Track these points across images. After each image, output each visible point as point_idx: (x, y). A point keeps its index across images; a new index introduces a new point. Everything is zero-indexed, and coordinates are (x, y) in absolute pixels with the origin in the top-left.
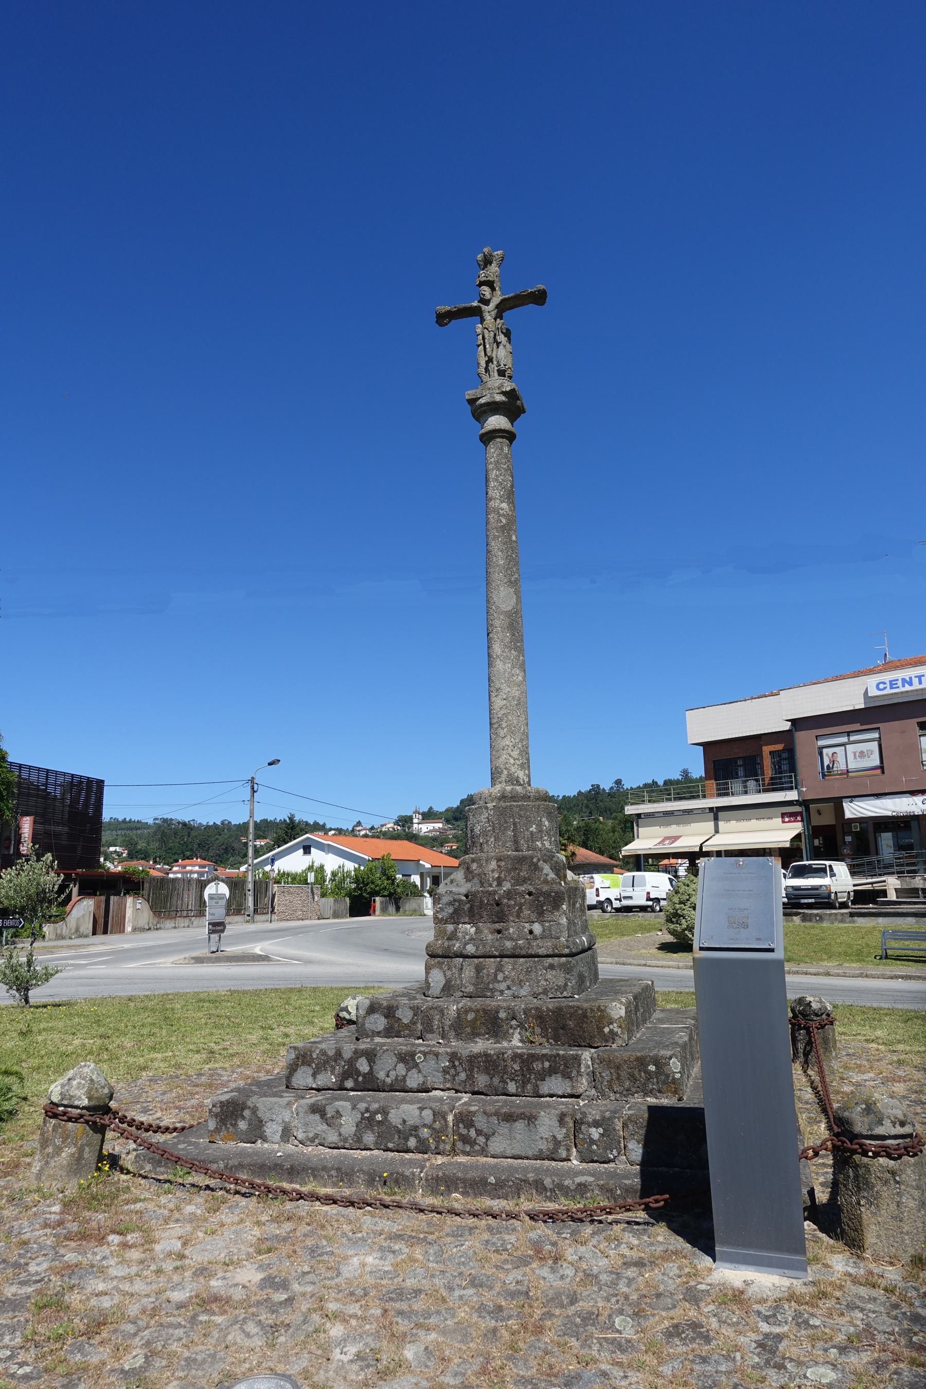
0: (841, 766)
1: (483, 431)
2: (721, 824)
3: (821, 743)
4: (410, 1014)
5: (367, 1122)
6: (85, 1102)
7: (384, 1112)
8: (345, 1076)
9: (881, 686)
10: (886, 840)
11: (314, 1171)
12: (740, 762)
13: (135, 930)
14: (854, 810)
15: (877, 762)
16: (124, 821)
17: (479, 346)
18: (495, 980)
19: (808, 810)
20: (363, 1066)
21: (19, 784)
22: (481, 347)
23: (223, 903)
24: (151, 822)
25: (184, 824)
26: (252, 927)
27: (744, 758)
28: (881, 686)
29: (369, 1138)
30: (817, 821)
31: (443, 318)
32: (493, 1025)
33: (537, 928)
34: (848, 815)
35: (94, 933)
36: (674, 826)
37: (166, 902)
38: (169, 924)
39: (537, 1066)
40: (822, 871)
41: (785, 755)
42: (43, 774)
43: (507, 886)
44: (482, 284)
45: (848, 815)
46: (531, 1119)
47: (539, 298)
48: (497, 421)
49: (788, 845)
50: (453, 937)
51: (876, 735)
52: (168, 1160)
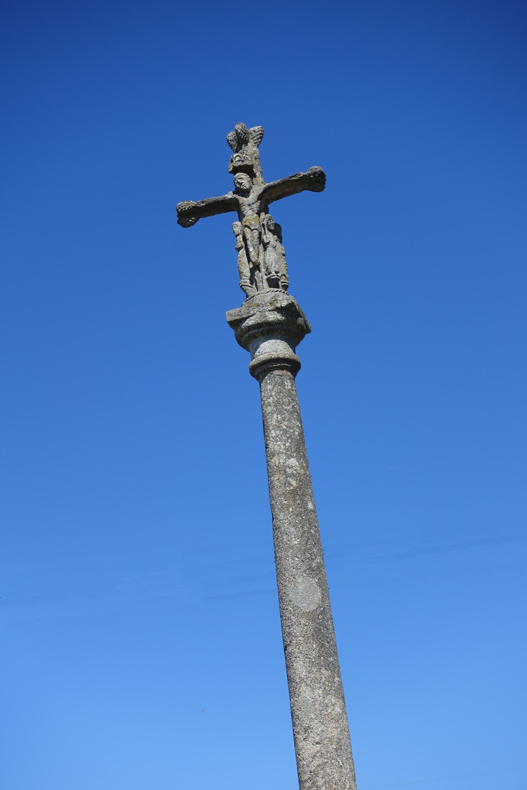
1: (254, 362)
17: (239, 249)
22: (243, 251)
31: (187, 217)
44: (236, 170)
47: (316, 182)
48: (272, 348)
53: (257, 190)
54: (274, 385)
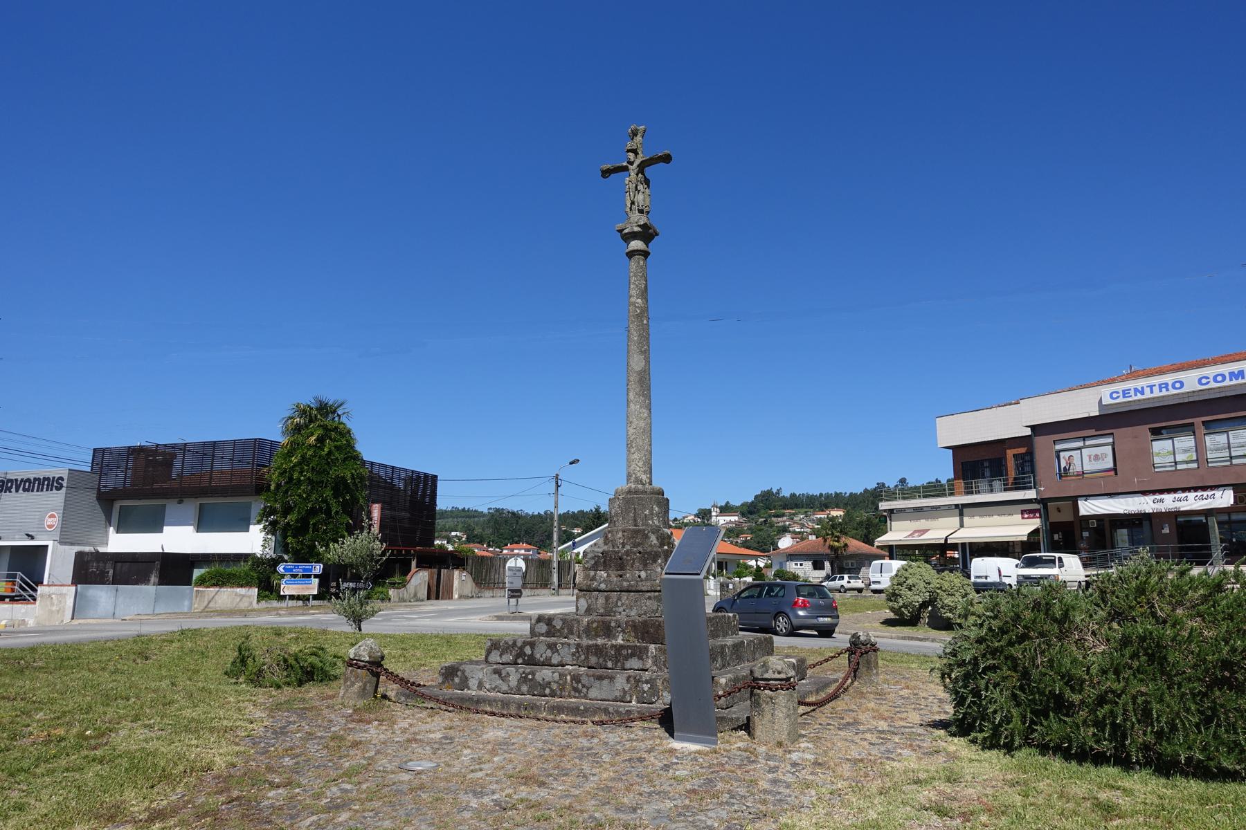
0: (1077, 467)
2: (966, 519)
3: (1058, 447)
4: (560, 623)
5: (524, 679)
6: (367, 659)
7: (533, 674)
8: (518, 656)
9: (1115, 395)
10: (1123, 534)
11: (490, 702)
12: (986, 464)
13: (460, 597)
14: (1088, 508)
15: (1111, 465)
16: (464, 510)
18: (617, 606)
19: (1046, 507)
20: (528, 650)
21: (371, 479)
23: (520, 574)
24: (486, 511)
25: (513, 513)
26: (556, 599)
27: (990, 460)
28: (1115, 395)
29: (524, 688)
30: (1055, 517)
31: (606, 173)
32: (608, 631)
33: (643, 574)
34: (1083, 512)
35: (429, 598)
36: (923, 521)
37: (486, 575)
38: (488, 593)
39: (624, 652)
40: (1051, 562)
41: (1027, 458)
42: (389, 470)
43: (628, 547)
45: (1083, 512)
46: (612, 679)
47: (667, 159)
48: (636, 244)
49: (1025, 539)
50: (593, 579)
51: (1110, 440)
52: (412, 690)
53: (637, 162)
54: (635, 264)
